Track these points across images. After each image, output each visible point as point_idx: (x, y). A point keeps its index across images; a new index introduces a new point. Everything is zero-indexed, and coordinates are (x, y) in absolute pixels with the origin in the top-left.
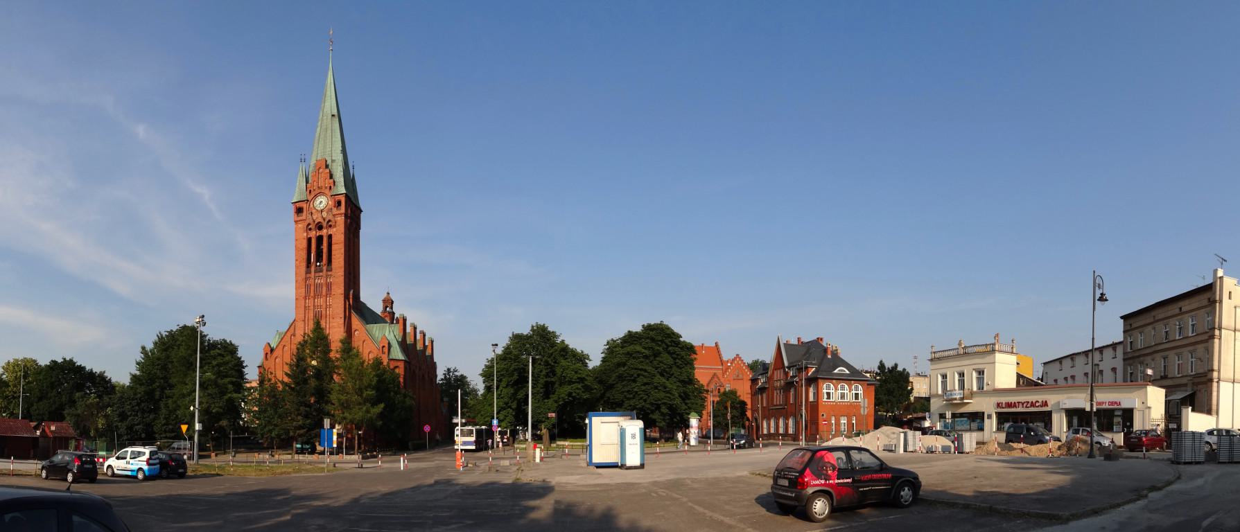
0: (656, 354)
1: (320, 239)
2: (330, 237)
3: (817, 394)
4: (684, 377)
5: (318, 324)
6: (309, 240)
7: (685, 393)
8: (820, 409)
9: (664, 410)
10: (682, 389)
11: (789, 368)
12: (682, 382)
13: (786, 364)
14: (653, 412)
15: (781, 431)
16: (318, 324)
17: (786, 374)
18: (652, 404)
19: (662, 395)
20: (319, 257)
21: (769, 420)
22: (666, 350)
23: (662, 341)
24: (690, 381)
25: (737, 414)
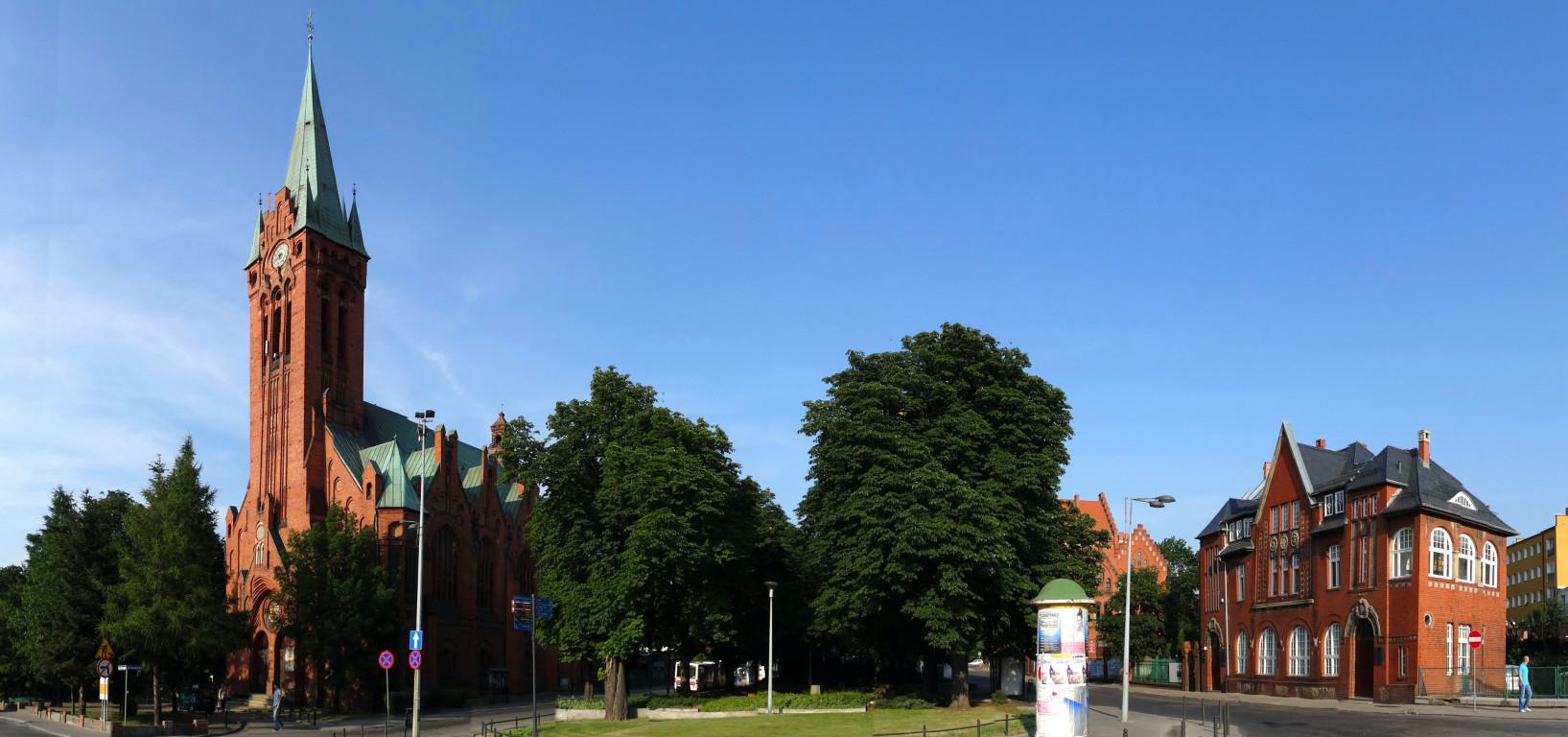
0: (936, 407)
1: (277, 313)
2: (289, 306)
3: (1415, 555)
4: (1026, 479)
5: (188, 450)
6: (265, 320)
7: (1030, 533)
8: (1424, 599)
9: (953, 583)
10: (1017, 520)
11: (1319, 496)
12: (1023, 493)
13: (1309, 488)
14: (915, 591)
15: (1295, 668)
16: (188, 450)
17: (1311, 513)
18: (906, 560)
19: (941, 525)
20: (275, 349)
21: (1252, 637)
22: (968, 395)
23: (957, 369)
24: (1039, 497)
25: (1154, 622)
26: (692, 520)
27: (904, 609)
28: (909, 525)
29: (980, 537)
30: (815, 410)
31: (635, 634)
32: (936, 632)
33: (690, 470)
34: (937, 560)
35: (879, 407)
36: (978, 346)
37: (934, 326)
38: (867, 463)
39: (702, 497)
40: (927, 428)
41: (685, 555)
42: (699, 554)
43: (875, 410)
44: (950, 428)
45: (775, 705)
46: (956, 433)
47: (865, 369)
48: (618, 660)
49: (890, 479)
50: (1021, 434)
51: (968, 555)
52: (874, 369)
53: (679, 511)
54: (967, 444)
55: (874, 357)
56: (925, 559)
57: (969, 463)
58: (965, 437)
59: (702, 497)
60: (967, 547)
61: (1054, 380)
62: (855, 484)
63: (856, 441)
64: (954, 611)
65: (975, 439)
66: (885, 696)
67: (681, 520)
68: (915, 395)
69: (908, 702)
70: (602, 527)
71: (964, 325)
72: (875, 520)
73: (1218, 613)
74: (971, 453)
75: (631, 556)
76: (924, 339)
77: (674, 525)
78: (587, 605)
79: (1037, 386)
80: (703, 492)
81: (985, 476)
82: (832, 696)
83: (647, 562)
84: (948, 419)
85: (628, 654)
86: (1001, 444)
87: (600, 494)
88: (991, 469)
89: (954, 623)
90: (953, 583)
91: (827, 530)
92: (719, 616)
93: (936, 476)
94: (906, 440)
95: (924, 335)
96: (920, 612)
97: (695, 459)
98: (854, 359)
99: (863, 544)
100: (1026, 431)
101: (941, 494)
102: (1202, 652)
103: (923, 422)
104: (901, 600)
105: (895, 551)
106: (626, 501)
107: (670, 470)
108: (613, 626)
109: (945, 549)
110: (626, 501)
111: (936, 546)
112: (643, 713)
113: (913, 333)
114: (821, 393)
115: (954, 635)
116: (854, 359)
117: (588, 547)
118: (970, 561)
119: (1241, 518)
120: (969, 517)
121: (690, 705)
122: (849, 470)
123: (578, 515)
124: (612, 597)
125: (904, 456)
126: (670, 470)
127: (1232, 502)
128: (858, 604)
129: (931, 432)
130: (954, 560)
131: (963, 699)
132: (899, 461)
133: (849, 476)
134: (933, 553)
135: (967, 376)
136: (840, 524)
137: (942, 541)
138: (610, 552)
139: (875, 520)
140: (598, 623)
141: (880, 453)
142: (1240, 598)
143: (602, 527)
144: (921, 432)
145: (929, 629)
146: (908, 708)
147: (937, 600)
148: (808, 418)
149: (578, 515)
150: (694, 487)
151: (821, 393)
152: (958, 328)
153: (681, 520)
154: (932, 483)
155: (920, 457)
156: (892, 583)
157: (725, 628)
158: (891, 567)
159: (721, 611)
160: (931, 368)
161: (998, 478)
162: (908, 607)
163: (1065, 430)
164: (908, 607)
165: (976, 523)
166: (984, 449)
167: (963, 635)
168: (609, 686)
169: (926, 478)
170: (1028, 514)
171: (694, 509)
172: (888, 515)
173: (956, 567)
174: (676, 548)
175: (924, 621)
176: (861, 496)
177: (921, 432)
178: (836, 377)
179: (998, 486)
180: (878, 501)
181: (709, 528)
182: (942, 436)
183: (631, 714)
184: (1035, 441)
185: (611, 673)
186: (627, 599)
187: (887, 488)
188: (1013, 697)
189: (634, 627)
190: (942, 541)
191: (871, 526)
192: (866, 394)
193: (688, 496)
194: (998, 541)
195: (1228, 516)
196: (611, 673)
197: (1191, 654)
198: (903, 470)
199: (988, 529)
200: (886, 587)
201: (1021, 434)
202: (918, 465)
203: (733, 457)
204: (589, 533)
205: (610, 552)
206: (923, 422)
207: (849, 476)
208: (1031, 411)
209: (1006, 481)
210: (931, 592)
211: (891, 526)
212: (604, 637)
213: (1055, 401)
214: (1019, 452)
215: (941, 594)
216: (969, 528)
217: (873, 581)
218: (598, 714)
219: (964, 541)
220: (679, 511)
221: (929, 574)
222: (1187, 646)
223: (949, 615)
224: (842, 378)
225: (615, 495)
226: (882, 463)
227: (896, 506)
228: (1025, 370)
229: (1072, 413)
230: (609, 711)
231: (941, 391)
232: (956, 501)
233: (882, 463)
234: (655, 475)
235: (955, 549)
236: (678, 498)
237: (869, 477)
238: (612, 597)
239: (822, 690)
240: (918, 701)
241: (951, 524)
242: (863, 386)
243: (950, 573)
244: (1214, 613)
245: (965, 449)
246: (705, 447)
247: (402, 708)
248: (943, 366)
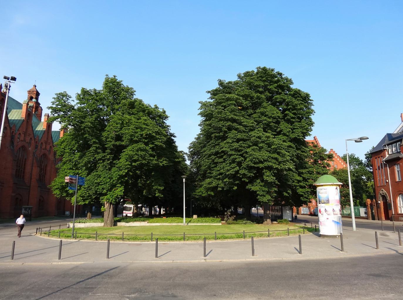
0: (256, 105)
9: (269, 177)
14: (252, 180)
18: (250, 168)
19: (264, 154)
22: (269, 99)
23: (265, 87)
26: (152, 149)
27: (247, 187)
28: (251, 155)
29: (280, 159)
30: (204, 105)
31: (119, 194)
32: (261, 196)
33: (152, 128)
34: (262, 169)
35: (235, 106)
36: (274, 76)
37: (253, 68)
38: (230, 129)
39: (157, 139)
40: (252, 114)
41: (149, 163)
42: (155, 162)
43: (233, 106)
44: (263, 114)
45: (186, 222)
46: (266, 116)
47: (224, 89)
48: (111, 203)
49: (239, 136)
50: (293, 116)
51: (275, 166)
52: (229, 88)
53: (146, 144)
54: (271, 120)
55: (230, 83)
56: (258, 168)
57: (271, 129)
58: (269, 118)
59: (157, 139)
60: (275, 163)
61: (304, 89)
62: (224, 138)
63: (228, 120)
64: (268, 188)
65: (274, 118)
66: (234, 220)
67: (148, 148)
68: (246, 100)
69: (244, 222)
70: (106, 149)
71: (268, 67)
72: (233, 153)
73: (386, 187)
74: (272, 124)
75: (123, 161)
76: (247, 74)
77: (145, 150)
78: (98, 181)
79: (297, 94)
80: (157, 137)
81: (279, 133)
82: (200, 219)
83: (131, 165)
84: (262, 110)
85: (116, 202)
86: (285, 120)
87: (105, 134)
88: (281, 131)
89: (268, 193)
90: (269, 177)
91: (210, 156)
92: (159, 188)
93: (261, 134)
94: (245, 120)
95: (247, 72)
96: (253, 188)
97: (154, 122)
98: (221, 83)
99: (228, 162)
100: (294, 114)
101: (263, 142)
102: (377, 203)
103: (250, 111)
104: (247, 184)
105: (244, 165)
106: (119, 138)
107: (144, 126)
108: (110, 190)
109: (266, 164)
110: (119, 138)
111: (262, 163)
112: (119, 224)
113: (242, 72)
114: (207, 98)
115: (268, 197)
116: (221, 83)
117: (98, 157)
118: (276, 168)
119: (396, 142)
120: (275, 151)
121: (144, 221)
122: (221, 131)
123: (94, 142)
124: (111, 178)
125: (245, 126)
126: (144, 126)
127: (389, 135)
128: (222, 185)
129: (254, 116)
130: (270, 168)
131: (269, 220)
132: (243, 129)
133: (221, 134)
134: (261, 166)
135: (269, 91)
136: (217, 153)
137: (265, 161)
138: (108, 160)
139: (233, 153)
140: (103, 189)
141: (235, 124)
142: (397, 180)
143: (106, 149)
144: (249, 116)
145: (258, 195)
146: (245, 224)
147: (261, 184)
148: (201, 108)
149: (94, 142)
150: (154, 134)
151: (207, 98)
152: (264, 69)
153: (148, 148)
154: (259, 137)
155: (253, 126)
156: (243, 178)
157: (160, 191)
158: (242, 172)
159: (160, 185)
160: (250, 86)
161: (284, 135)
162: (249, 187)
163: (311, 112)
164: (249, 187)
165: (278, 153)
166: (278, 123)
167: (272, 197)
168: (106, 214)
169: (257, 135)
170: (297, 149)
171: (153, 143)
172: (239, 151)
173: (270, 171)
174: (145, 159)
175: (256, 192)
176: (228, 143)
177: (249, 116)
178: (213, 91)
179: (285, 138)
180: (236, 145)
181: (159, 152)
182: (260, 117)
183: (115, 225)
184: (299, 118)
185: (107, 209)
186: (118, 179)
187: (238, 141)
188: (290, 221)
189: (119, 191)
190: (265, 161)
191: (231, 155)
192: (228, 99)
193: (150, 138)
194: (287, 161)
195: (387, 142)
196: (107, 209)
197: (371, 205)
198: (244, 132)
199: (283, 156)
200: (240, 179)
201: (293, 116)
202: (251, 130)
203: (167, 122)
204: (99, 151)
205: (108, 160)
206: (250, 111)
207: (221, 134)
208: (296, 105)
209: (287, 136)
210: (258, 181)
211: (242, 155)
212: (106, 194)
213: (305, 99)
214: (292, 123)
215: (263, 181)
216: (276, 156)
217: (234, 177)
218: (101, 224)
219: (274, 161)
220: (146, 144)
221: (259, 174)
222: (369, 201)
223: (267, 189)
224: (214, 93)
225: (113, 134)
226: (236, 129)
227: (244, 147)
228: (291, 86)
229: (313, 103)
230: (106, 223)
231: (258, 98)
232: (269, 145)
233: (236, 129)
234: (137, 128)
235: (270, 164)
236: (146, 138)
237: (232, 134)
238: (111, 178)
239: (198, 217)
240: (249, 221)
241: (268, 154)
242: (228, 96)
243: (268, 173)
244: (383, 186)
245: (270, 122)
246: (158, 117)
247: (73, 218)
248: (258, 86)
